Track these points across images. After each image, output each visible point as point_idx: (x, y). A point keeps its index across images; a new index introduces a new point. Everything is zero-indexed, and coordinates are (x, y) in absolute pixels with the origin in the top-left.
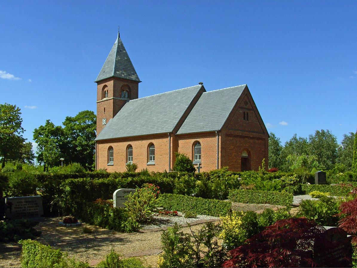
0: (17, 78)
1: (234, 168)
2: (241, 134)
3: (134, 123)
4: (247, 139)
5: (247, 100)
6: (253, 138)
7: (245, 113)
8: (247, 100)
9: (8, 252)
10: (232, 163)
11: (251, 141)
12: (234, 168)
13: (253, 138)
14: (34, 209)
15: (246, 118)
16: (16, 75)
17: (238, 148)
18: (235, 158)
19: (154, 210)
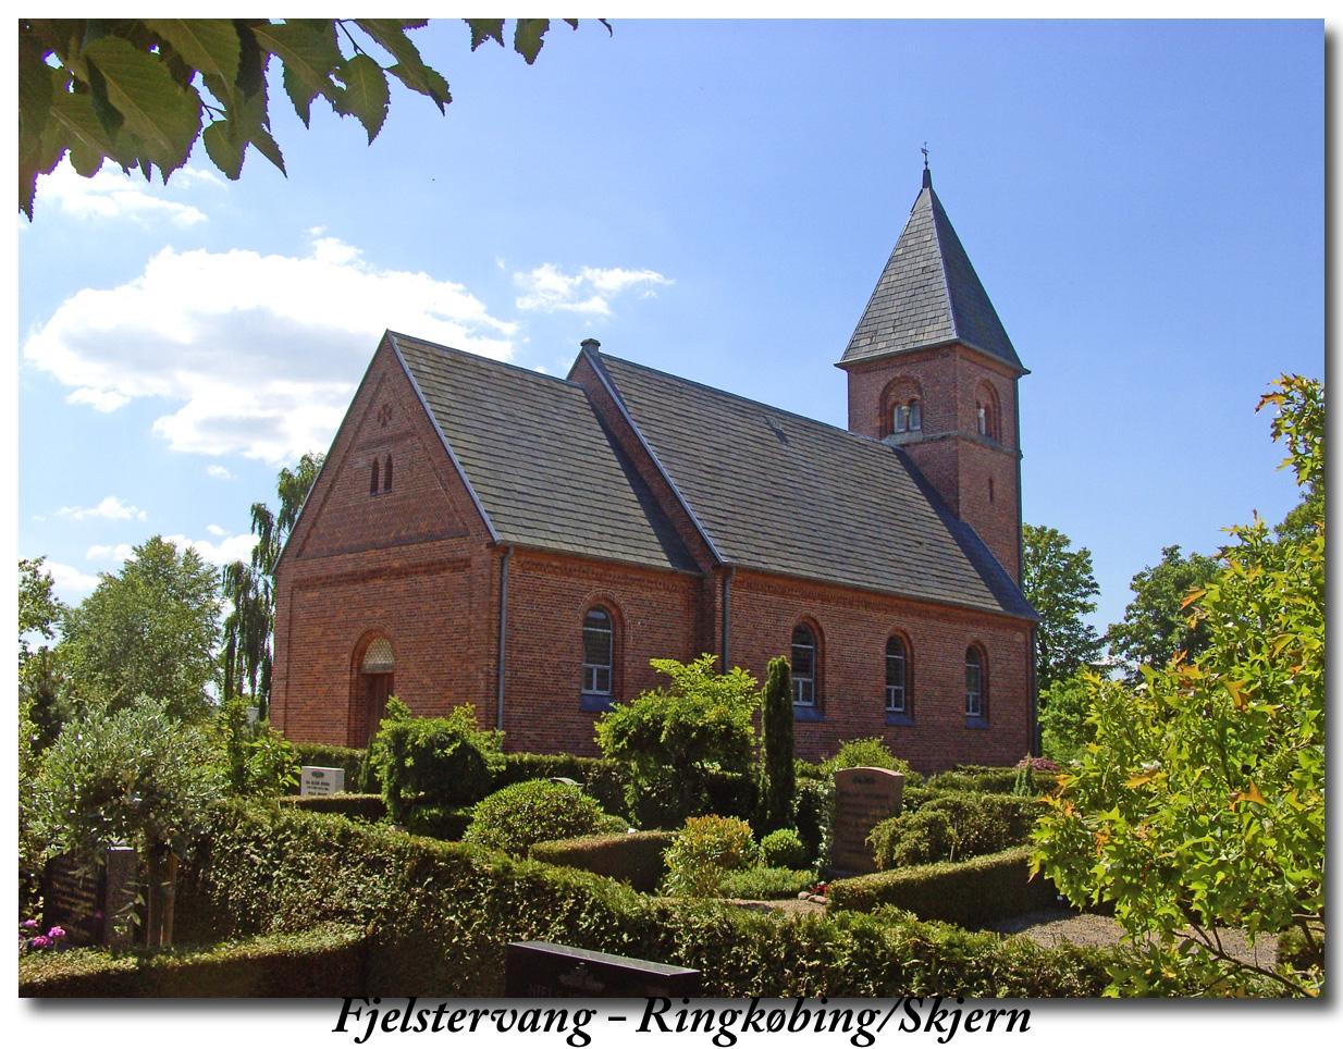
0: (671, 282)
1: (322, 724)
2: (350, 567)
3: (893, 336)
4: (379, 582)
5: (372, 416)
6: (400, 573)
7: (380, 461)
8: (372, 416)
9: (993, 766)
10: (313, 702)
11: (400, 586)
12: (322, 724)
13: (400, 573)
14: (319, 794)
15: (381, 485)
16: (667, 277)
17: (339, 631)
18: (325, 680)
19: (41, 898)
